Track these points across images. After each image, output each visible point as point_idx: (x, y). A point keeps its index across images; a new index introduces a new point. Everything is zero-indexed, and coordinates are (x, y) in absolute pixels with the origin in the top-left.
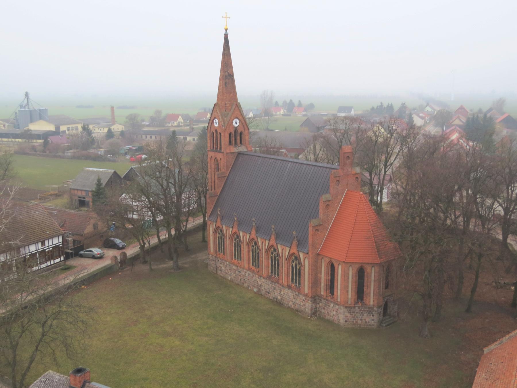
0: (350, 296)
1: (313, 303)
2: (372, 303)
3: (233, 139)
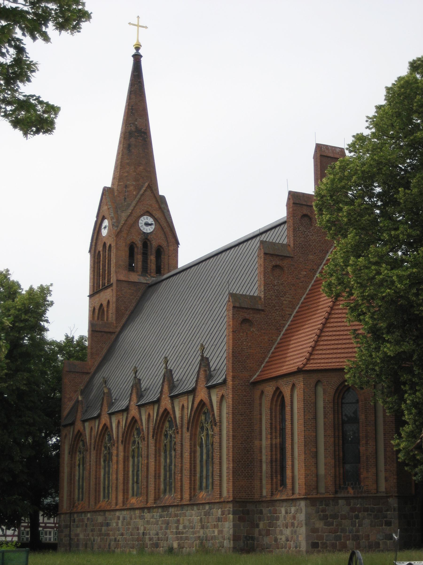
0: (322, 471)
1: (241, 519)
2: (383, 486)
3: (139, 257)
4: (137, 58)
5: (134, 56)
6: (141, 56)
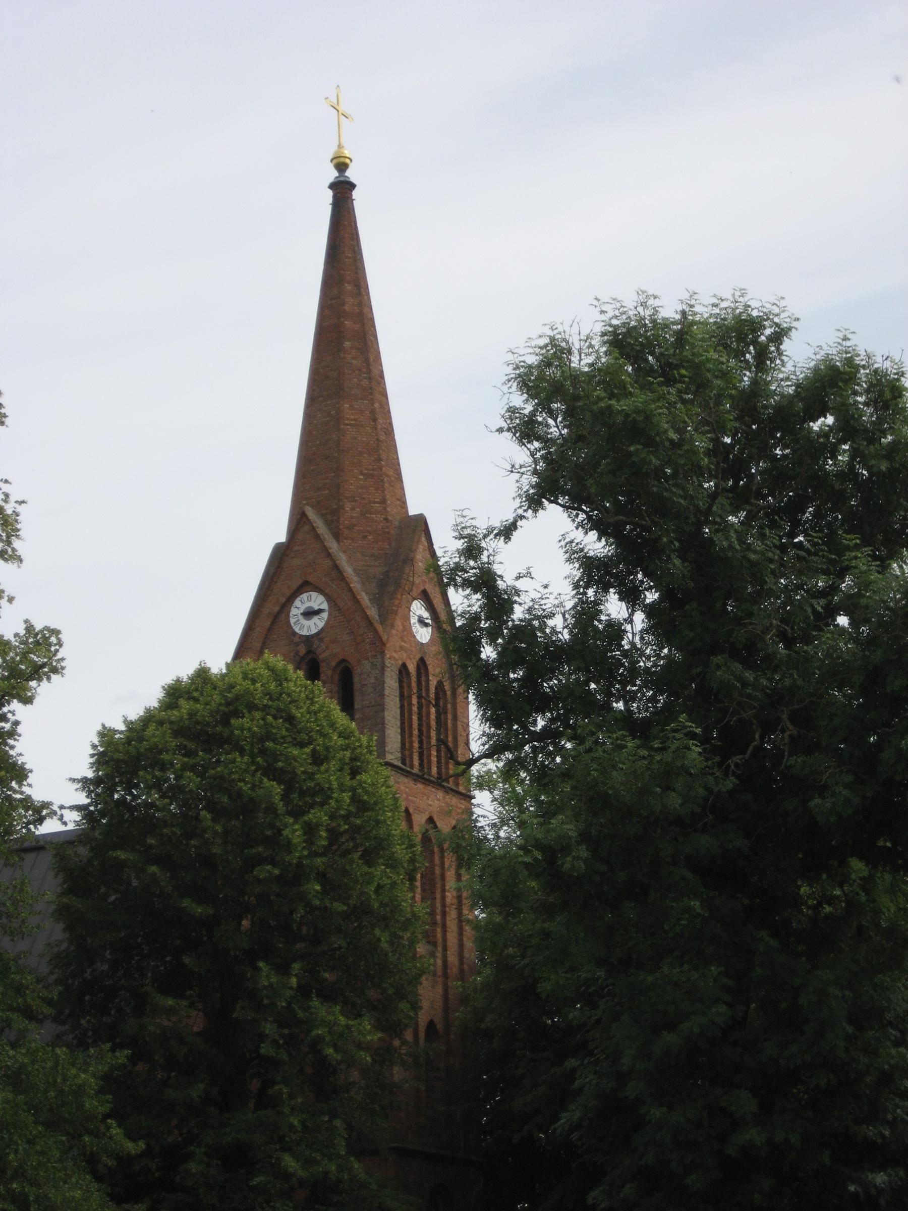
4: (342, 191)
5: (332, 186)
6: (352, 186)
